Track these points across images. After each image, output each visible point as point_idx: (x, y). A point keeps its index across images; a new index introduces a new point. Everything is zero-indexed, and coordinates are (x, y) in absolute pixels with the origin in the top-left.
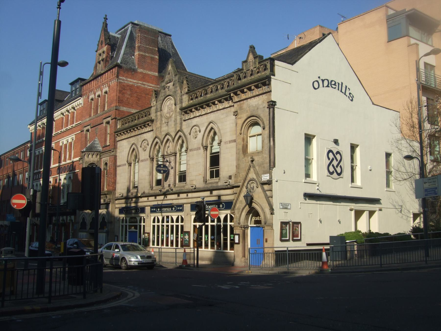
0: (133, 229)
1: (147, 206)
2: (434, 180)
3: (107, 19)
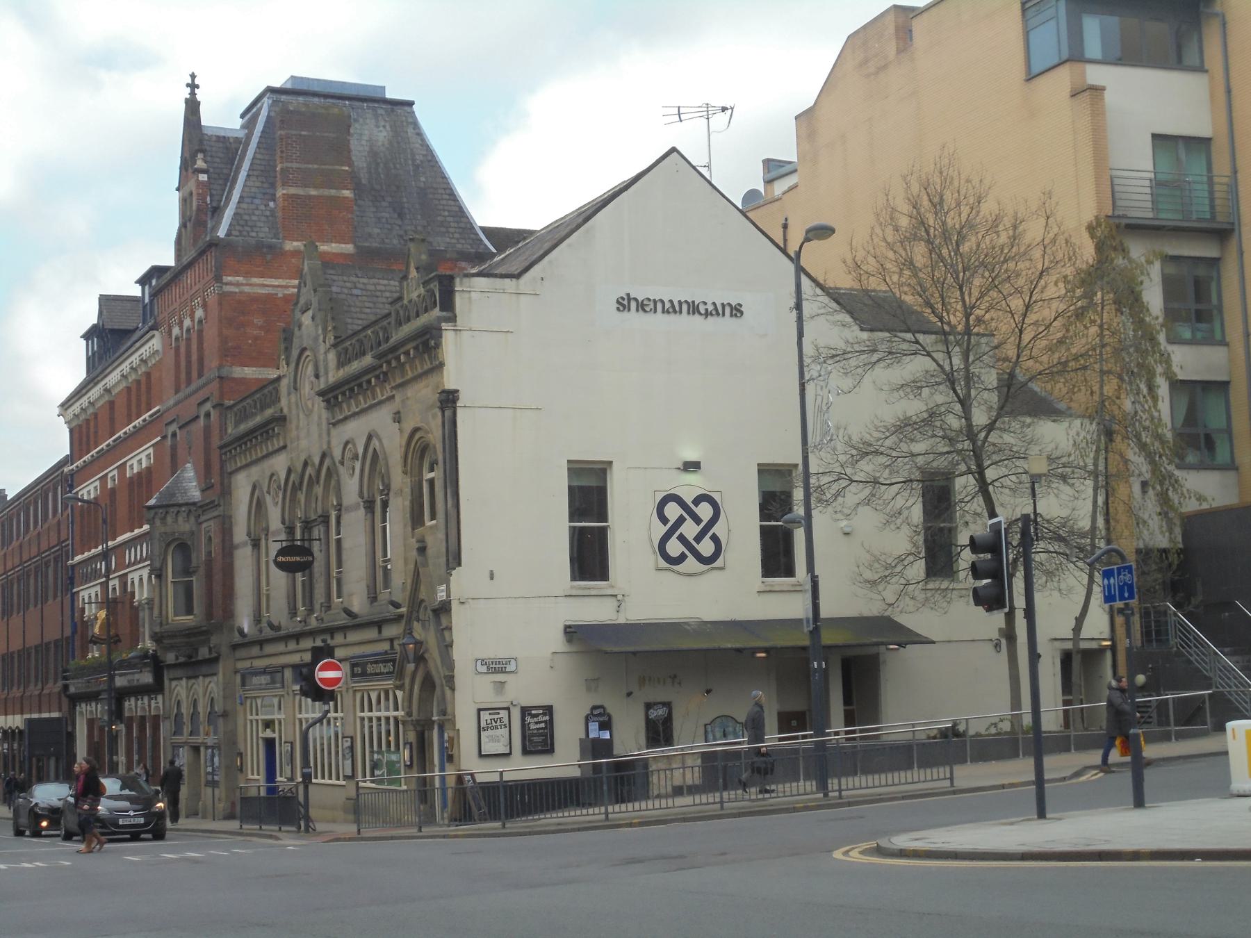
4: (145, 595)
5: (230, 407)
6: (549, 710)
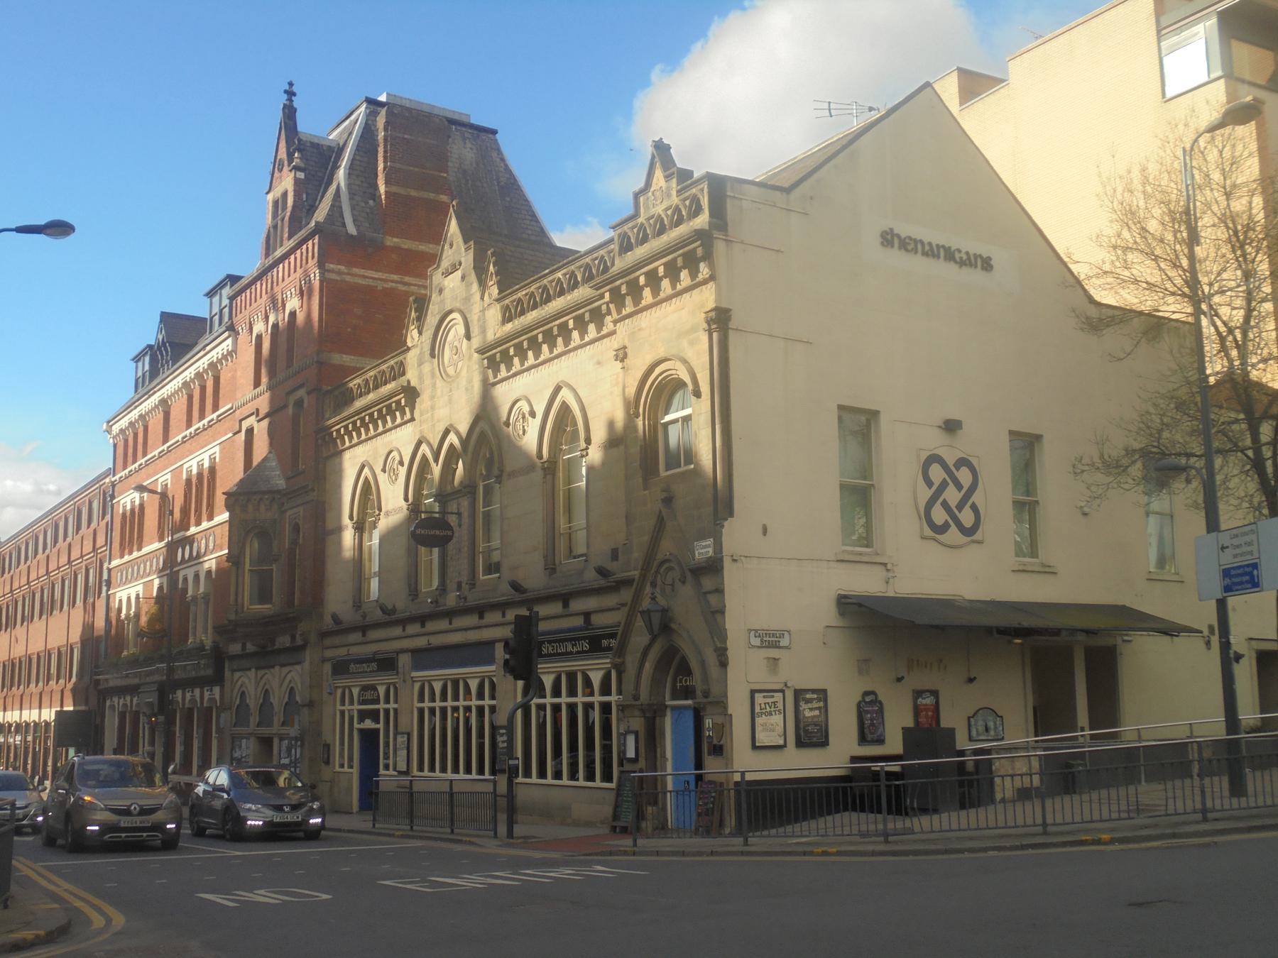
0: (369, 724)
1: (403, 651)
2: (1248, 539)
3: (294, 94)
4: (202, 590)
5: (330, 392)
6: (822, 694)
